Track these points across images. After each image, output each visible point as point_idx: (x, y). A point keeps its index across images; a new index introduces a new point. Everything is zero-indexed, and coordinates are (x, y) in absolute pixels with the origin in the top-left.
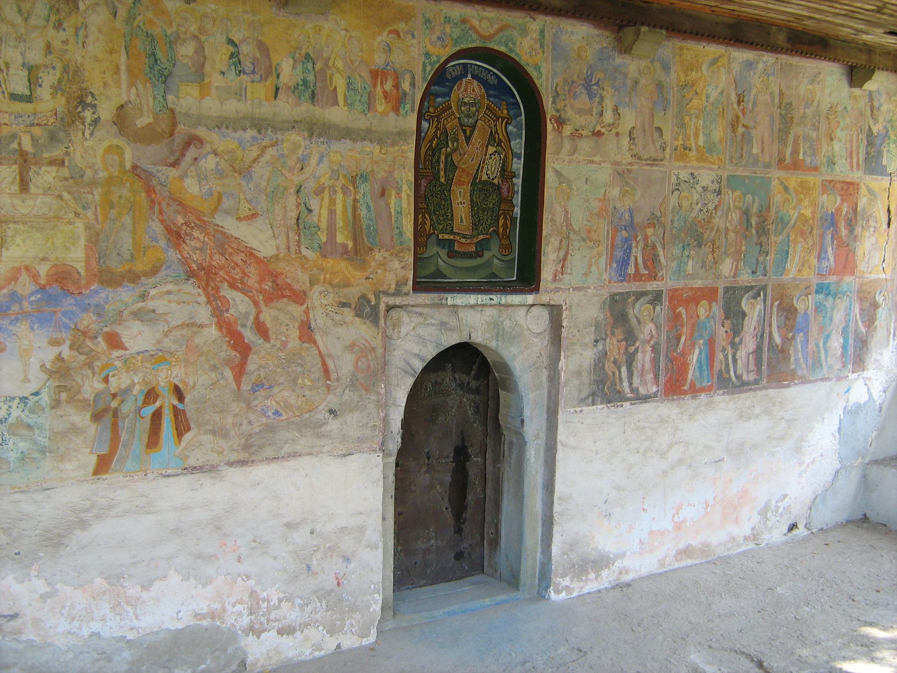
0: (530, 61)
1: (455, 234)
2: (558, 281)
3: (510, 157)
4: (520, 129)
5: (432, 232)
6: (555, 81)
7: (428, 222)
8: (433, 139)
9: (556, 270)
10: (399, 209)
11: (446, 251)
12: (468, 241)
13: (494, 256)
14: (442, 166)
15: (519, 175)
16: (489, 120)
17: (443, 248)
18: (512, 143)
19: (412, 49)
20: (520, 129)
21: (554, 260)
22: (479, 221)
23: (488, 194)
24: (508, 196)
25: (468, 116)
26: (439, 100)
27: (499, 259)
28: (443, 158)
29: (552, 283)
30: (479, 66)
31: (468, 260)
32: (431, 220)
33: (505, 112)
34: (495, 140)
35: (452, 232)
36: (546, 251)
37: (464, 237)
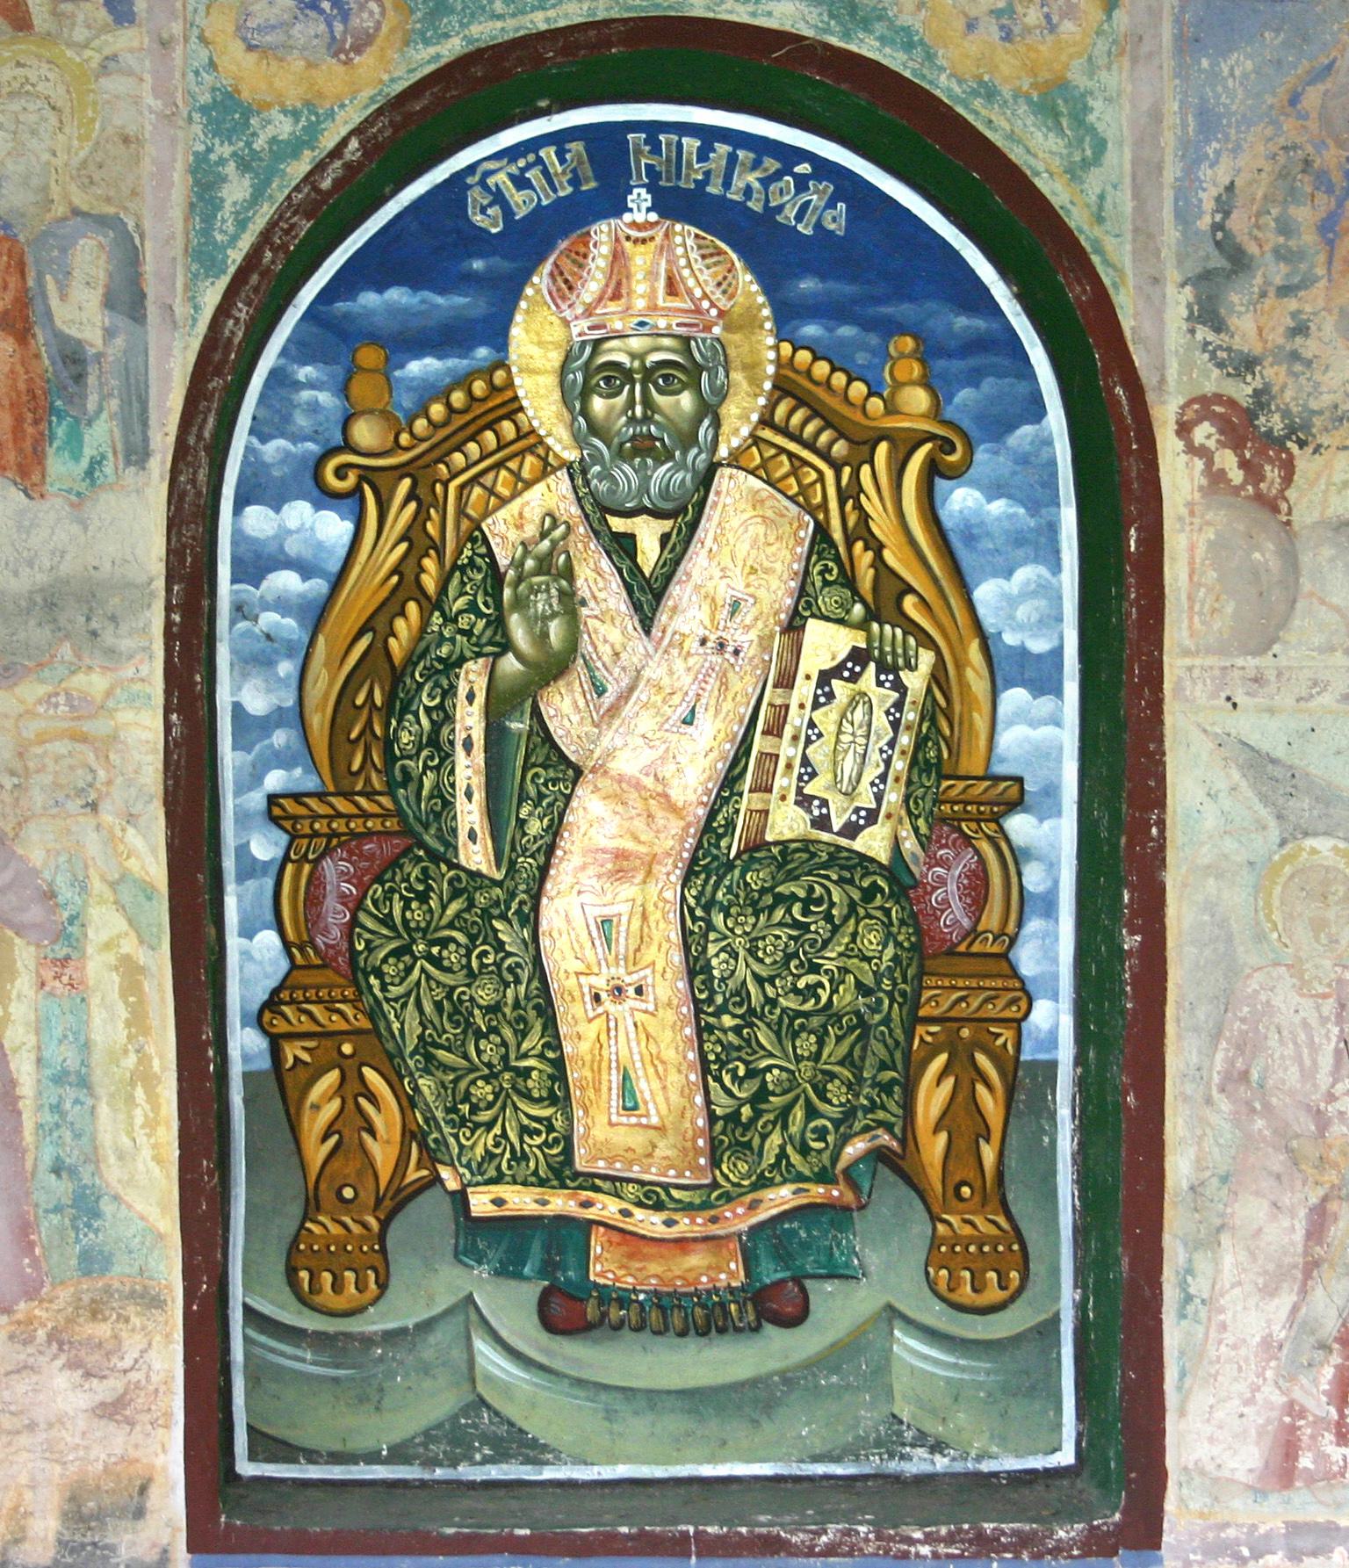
0: (1008, 69)
1: (590, 1181)
2: (1311, 1479)
3: (977, 682)
4: (1041, 498)
5: (413, 1174)
6: (1213, 178)
7: (387, 1118)
8: (391, 606)
9: (1294, 1410)
10: (67, 1056)
11: (530, 1291)
12: (685, 1226)
13: (892, 1314)
14: (468, 770)
15: (1051, 791)
16: (798, 463)
17: (509, 1270)
18: (986, 593)
19: (114, 85)
20: (1041, 498)
21: (1269, 1346)
22: (762, 1095)
23: (820, 928)
24: (973, 933)
25: (643, 448)
26: (419, 368)
27: (932, 1335)
28: (470, 719)
29: (1258, 1491)
30: (709, 135)
31: (692, 1343)
32: (409, 1102)
33: (918, 399)
34: (849, 580)
35: (562, 1173)
36: (1199, 1286)
37: (654, 1197)
